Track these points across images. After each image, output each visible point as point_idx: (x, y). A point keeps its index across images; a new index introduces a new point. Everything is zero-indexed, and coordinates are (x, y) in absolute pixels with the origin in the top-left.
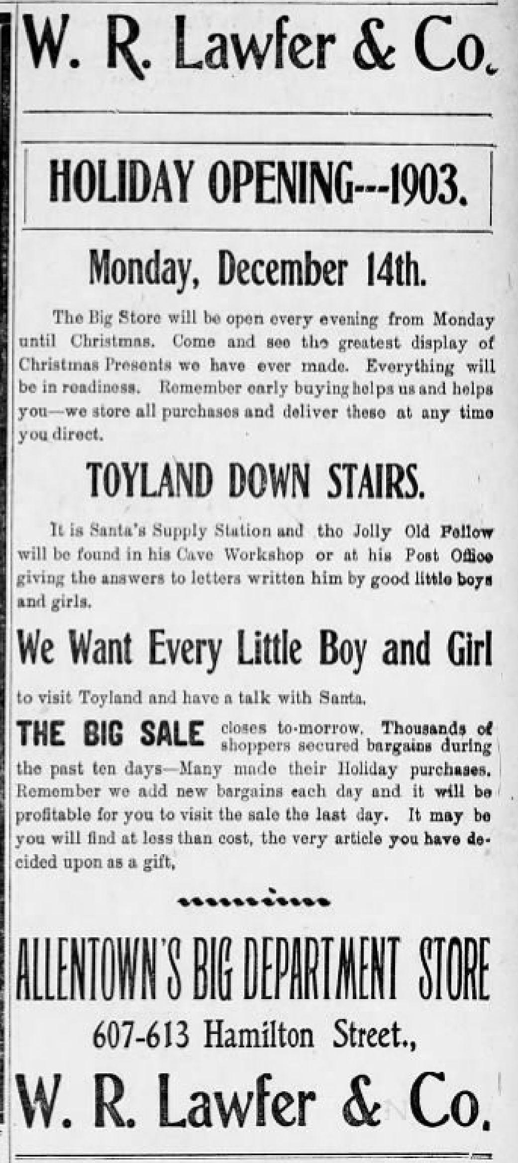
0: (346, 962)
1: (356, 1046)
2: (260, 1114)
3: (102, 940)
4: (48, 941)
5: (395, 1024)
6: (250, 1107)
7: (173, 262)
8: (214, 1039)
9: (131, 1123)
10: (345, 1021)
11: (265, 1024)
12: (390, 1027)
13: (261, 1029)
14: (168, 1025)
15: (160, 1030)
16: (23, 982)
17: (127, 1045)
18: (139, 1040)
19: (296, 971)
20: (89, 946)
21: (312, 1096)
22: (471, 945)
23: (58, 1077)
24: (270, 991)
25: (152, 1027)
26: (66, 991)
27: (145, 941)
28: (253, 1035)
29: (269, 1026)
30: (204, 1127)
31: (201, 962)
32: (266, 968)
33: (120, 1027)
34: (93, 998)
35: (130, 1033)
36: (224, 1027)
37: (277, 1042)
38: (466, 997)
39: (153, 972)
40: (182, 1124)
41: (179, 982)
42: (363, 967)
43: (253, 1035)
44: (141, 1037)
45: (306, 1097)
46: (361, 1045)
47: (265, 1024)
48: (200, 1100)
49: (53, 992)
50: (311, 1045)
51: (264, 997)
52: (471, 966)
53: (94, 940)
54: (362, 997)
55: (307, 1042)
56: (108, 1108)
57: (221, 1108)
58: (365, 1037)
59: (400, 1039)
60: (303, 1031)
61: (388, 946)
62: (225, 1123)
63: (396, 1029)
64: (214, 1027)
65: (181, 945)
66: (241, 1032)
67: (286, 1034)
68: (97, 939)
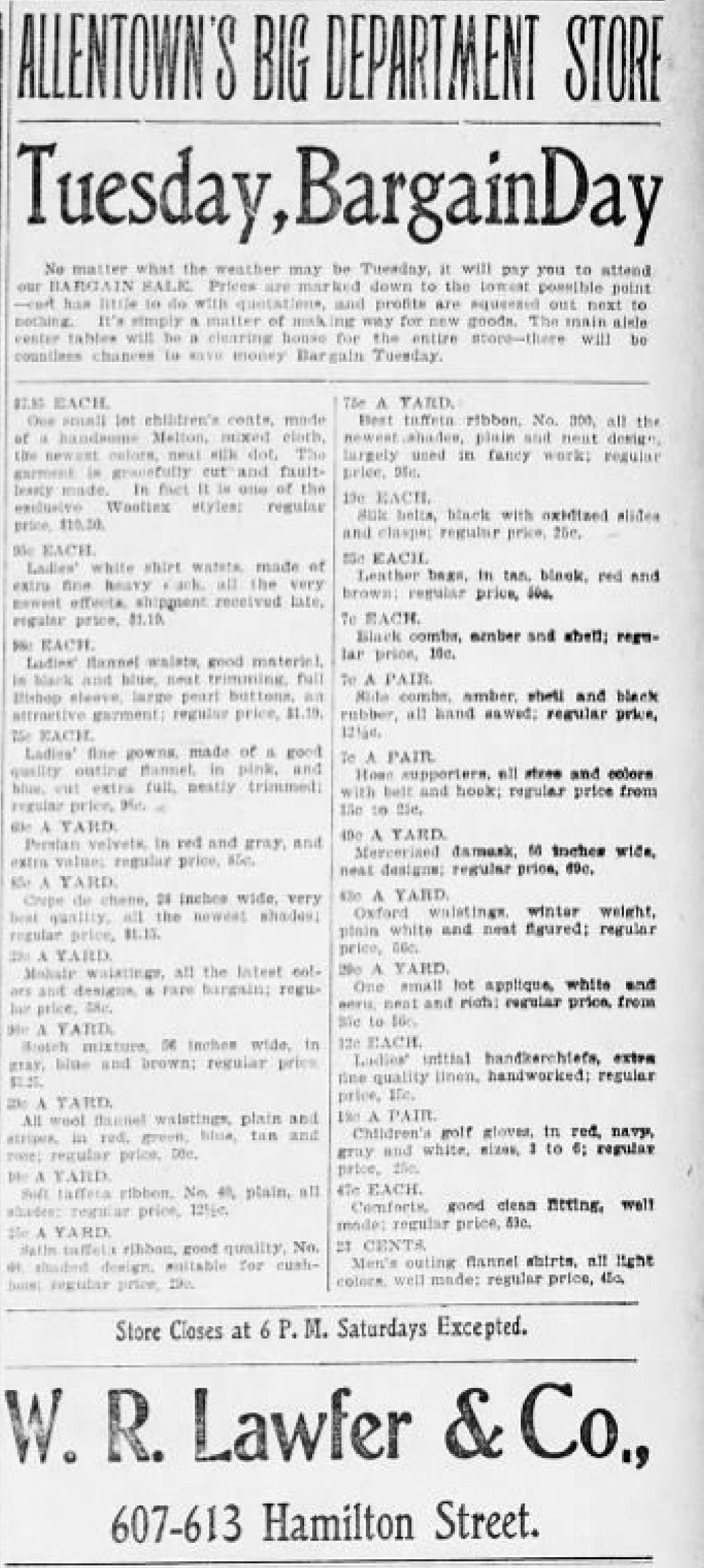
0: (465, 51)
1: (469, 1538)
2: (338, 1443)
3: (130, 20)
4: (57, 17)
5: (523, 1507)
6: (322, 1433)
7: (261, 1421)
8: (276, 1529)
9: (158, 1456)
10: (450, 1503)
11: (347, 1508)
12: (517, 1512)
13: (342, 1515)
14: (211, 1511)
15: (202, 1518)
16: (398, 74)
17: (158, 1540)
18: (174, 1532)
19: (398, 61)
20: (112, 25)
21: (407, 1418)
22: (639, 25)
23: (57, 1393)
24: (362, 88)
25: (191, 1515)
26: (81, 87)
27: (189, 18)
28: (331, 1523)
29: (352, 1511)
30: (257, 1461)
31: (265, 49)
32: (355, 56)
33: (150, 1514)
34: (118, 95)
35: (162, 1526)
36: (290, 1513)
37: (363, 1533)
38: (632, 97)
39: (198, 63)
40: (226, 1456)
41: (233, 77)
42: (490, 56)
43: (331, 1523)
44: (176, 1527)
45: (399, 1419)
46: (476, 1536)
47: (347, 1508)
48: (252, 1424)
49: (64, 87)
50: (410, 1537)
51: (353, 96)
52: (638, 54)
53: (120, 17)
54: (488, 97)
55: (405, 1533)
56: (126, 1436)
57: (281, 1434)
58: (482, 1526)
59: (529, 1528)
60: (399, 1518)
61: (526, 25)
62: (287, 1455)
63: (523, 1514)
64: (276, 1513)
65: (237, 27)
66: (315, 1519)
67: (374, 1522)
68: (125, 17)
